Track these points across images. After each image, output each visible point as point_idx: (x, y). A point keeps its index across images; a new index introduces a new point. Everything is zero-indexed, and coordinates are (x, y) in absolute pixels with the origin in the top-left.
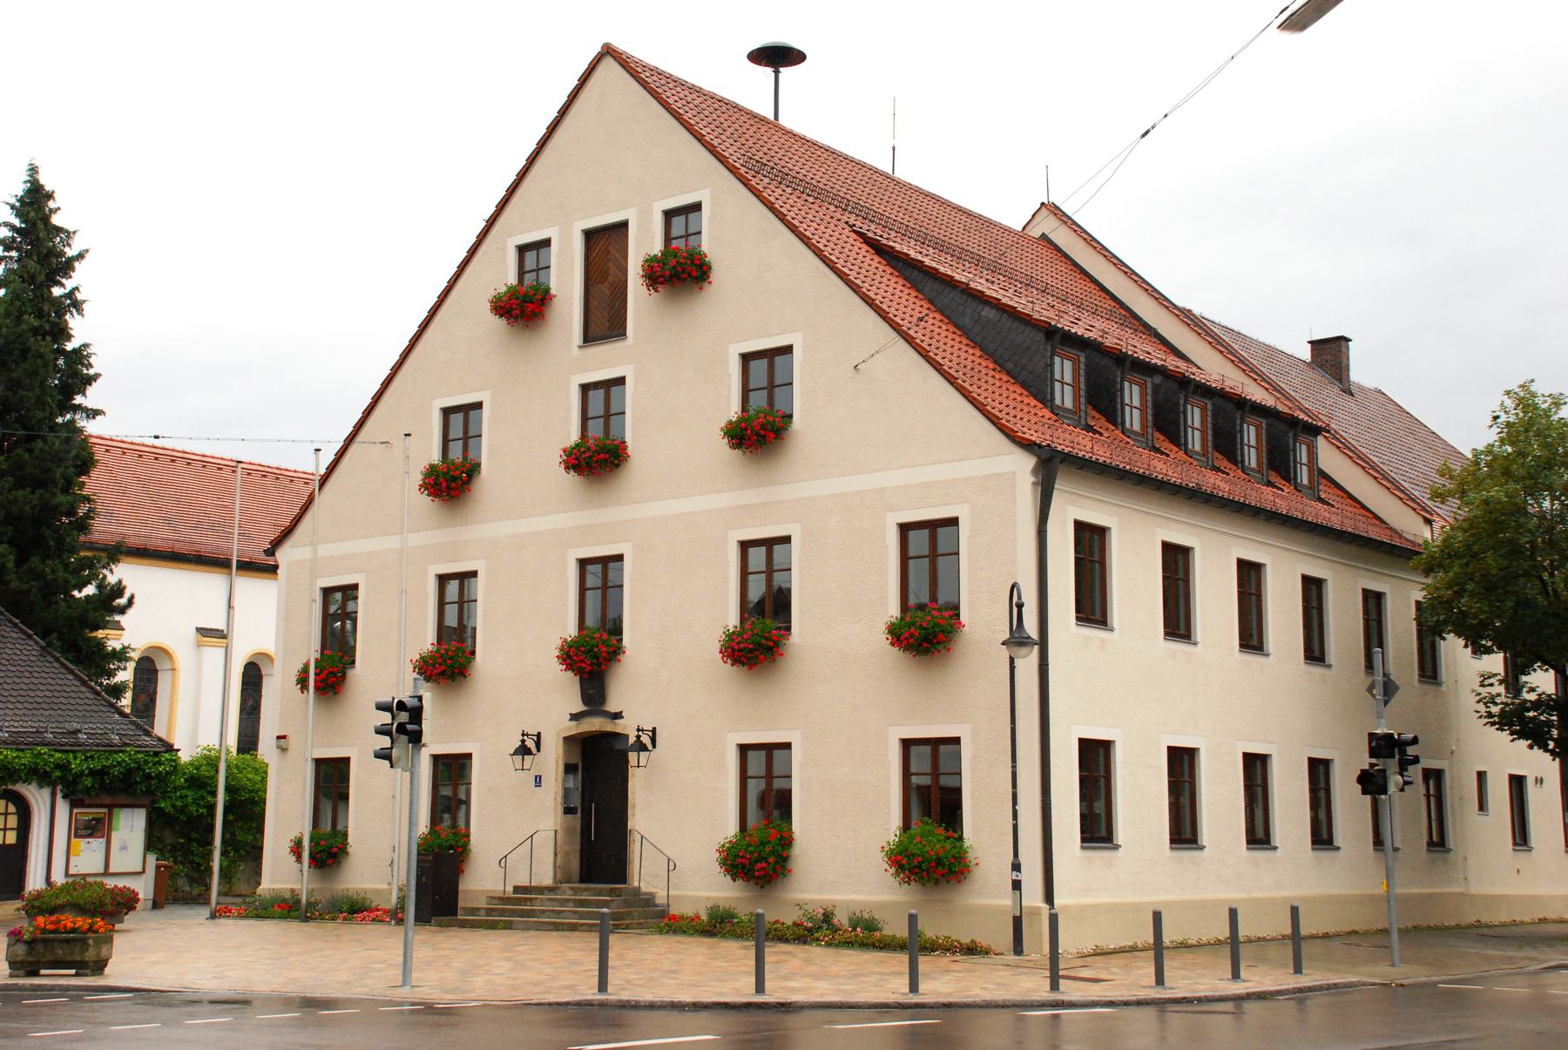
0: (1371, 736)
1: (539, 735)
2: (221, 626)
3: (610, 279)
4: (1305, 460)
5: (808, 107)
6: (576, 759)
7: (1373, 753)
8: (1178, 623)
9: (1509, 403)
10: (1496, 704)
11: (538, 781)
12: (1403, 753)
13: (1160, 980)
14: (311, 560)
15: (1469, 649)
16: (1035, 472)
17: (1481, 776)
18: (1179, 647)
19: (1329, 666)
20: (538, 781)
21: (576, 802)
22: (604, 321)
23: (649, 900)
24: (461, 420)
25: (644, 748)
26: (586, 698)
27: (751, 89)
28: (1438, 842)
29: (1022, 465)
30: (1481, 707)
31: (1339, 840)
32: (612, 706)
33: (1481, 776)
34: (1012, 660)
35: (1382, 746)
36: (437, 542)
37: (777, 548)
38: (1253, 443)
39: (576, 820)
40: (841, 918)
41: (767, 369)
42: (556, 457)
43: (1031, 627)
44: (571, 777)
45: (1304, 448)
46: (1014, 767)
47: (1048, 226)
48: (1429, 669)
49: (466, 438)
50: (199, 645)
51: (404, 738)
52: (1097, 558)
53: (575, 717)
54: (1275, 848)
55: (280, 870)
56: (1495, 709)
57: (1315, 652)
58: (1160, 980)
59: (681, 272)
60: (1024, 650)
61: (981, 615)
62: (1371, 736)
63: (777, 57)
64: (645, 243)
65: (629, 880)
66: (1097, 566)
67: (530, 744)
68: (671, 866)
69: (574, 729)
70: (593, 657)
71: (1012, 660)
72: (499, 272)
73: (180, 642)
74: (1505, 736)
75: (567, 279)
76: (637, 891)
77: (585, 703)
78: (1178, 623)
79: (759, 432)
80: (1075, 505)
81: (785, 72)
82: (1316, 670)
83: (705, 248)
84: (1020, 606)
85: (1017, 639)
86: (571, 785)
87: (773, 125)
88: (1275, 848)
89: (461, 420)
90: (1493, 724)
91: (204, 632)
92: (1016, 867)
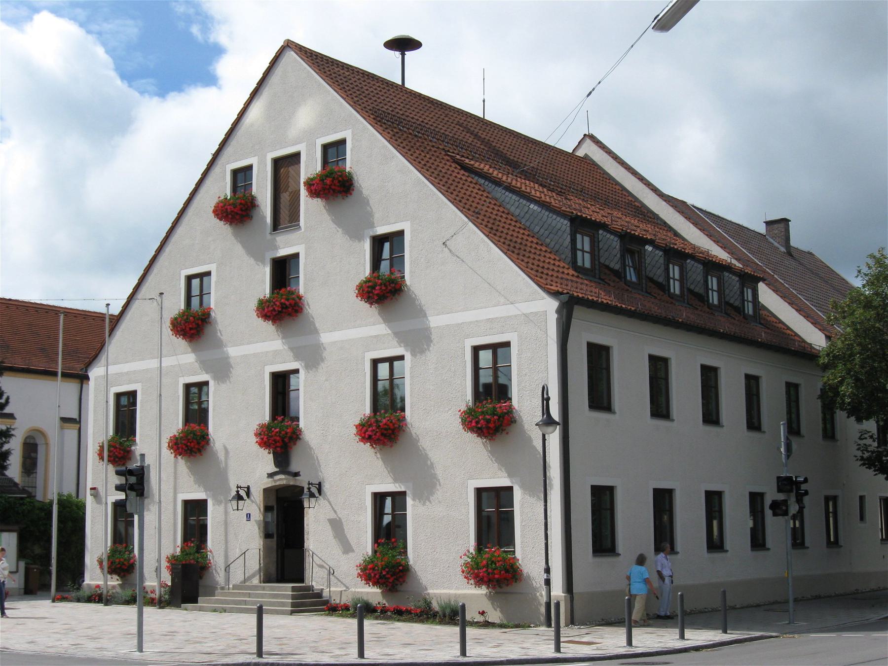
0: (778, 478)
1: (248, 488)
2: (75, 415)
3: (290, 190)
4: (750, 298)
5: (423, 77)
6: (273, 503)
7: (780, 490)
8: (660, 407)
9: (871, 262)
10: (868, 452)
11: (249, 516)
12: (798, 489)
13: (630, 643)
14: (109, 375)
15: (853, 418)
16: (559, 311)
17: (862, 498)
18: (661, 423)
19: (764, 432)
20: (249, 516)
21: (273, 529)
22: (285, 216)
23: (319, 595)
24: (197, 282)
25: (312, 495)
26: (277, 463)
27: (386, 66)
28: (834, 544)
29: (549, 306)
30: (859, 453)
31: (769, 543)
32: (294, 467)
33: (862, 498)
34: (544, 436)
35: (786, 484)
36: (183, 362)
37: (396, 363)
38: (715, 288)
39: (273, 542)
40: (435, 606)
41: (387, 246)
42: (254, 304)
43: (555, 412)
44: (269, 515)
45: (750, 291)
46: (546, 506)
47: (589, 150)
48: (829, 433)
49: (201, 295)
50: (62, 428)
51: (134, 493)
52: (604, 366)
53: (271, 475)
54: (727, 551)
55: (94, 576)
56: (866, 455)
57: (754, 424)
58: (630, 643)
59: (335, 185)
60: (550, 429)
61: (525, 402)
62: (778, 478)
63: (403, 45)
64: (311, 166)
65: (306, 581)
66: (604, 371)
67: (243, 493)
68: (331, 573)
69: (269, 483)
70: (281, 435)
71: (544, 436)
72: (221, 187)
73: (51, 428)
74: (871, 472)
75: (262, 189)
76: (310, 588)
77: (276, 465)
78: (660, 407)
79: (383, 289)
80: (591, 329)
81: (409, 54)
82: (755, 435)
83: (349, 166)
84: (548, 399)
85: (548, 421)
86: (269, 519)
87: (401, 89)
88: (727, 551)
89: (197, 282)
90: (863, 464)
91: (65, 420)
92: (548, 570)
